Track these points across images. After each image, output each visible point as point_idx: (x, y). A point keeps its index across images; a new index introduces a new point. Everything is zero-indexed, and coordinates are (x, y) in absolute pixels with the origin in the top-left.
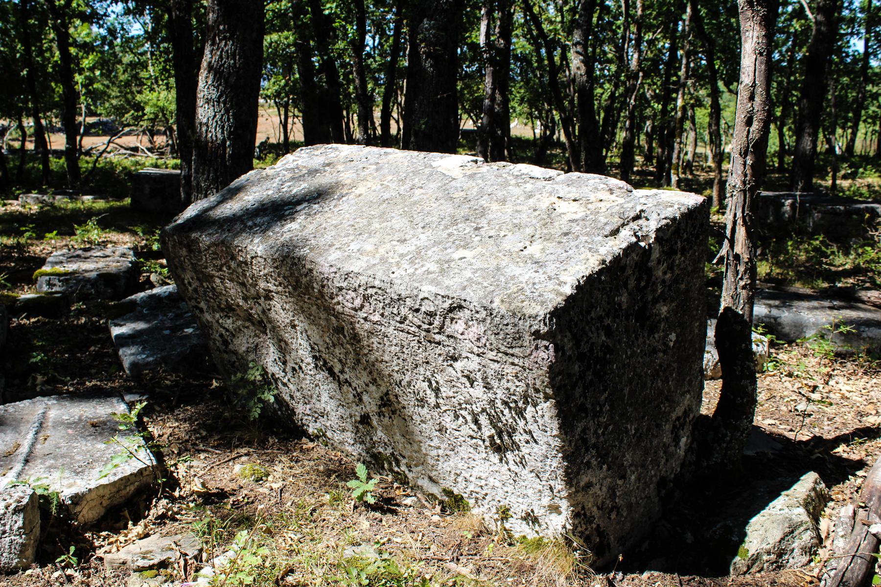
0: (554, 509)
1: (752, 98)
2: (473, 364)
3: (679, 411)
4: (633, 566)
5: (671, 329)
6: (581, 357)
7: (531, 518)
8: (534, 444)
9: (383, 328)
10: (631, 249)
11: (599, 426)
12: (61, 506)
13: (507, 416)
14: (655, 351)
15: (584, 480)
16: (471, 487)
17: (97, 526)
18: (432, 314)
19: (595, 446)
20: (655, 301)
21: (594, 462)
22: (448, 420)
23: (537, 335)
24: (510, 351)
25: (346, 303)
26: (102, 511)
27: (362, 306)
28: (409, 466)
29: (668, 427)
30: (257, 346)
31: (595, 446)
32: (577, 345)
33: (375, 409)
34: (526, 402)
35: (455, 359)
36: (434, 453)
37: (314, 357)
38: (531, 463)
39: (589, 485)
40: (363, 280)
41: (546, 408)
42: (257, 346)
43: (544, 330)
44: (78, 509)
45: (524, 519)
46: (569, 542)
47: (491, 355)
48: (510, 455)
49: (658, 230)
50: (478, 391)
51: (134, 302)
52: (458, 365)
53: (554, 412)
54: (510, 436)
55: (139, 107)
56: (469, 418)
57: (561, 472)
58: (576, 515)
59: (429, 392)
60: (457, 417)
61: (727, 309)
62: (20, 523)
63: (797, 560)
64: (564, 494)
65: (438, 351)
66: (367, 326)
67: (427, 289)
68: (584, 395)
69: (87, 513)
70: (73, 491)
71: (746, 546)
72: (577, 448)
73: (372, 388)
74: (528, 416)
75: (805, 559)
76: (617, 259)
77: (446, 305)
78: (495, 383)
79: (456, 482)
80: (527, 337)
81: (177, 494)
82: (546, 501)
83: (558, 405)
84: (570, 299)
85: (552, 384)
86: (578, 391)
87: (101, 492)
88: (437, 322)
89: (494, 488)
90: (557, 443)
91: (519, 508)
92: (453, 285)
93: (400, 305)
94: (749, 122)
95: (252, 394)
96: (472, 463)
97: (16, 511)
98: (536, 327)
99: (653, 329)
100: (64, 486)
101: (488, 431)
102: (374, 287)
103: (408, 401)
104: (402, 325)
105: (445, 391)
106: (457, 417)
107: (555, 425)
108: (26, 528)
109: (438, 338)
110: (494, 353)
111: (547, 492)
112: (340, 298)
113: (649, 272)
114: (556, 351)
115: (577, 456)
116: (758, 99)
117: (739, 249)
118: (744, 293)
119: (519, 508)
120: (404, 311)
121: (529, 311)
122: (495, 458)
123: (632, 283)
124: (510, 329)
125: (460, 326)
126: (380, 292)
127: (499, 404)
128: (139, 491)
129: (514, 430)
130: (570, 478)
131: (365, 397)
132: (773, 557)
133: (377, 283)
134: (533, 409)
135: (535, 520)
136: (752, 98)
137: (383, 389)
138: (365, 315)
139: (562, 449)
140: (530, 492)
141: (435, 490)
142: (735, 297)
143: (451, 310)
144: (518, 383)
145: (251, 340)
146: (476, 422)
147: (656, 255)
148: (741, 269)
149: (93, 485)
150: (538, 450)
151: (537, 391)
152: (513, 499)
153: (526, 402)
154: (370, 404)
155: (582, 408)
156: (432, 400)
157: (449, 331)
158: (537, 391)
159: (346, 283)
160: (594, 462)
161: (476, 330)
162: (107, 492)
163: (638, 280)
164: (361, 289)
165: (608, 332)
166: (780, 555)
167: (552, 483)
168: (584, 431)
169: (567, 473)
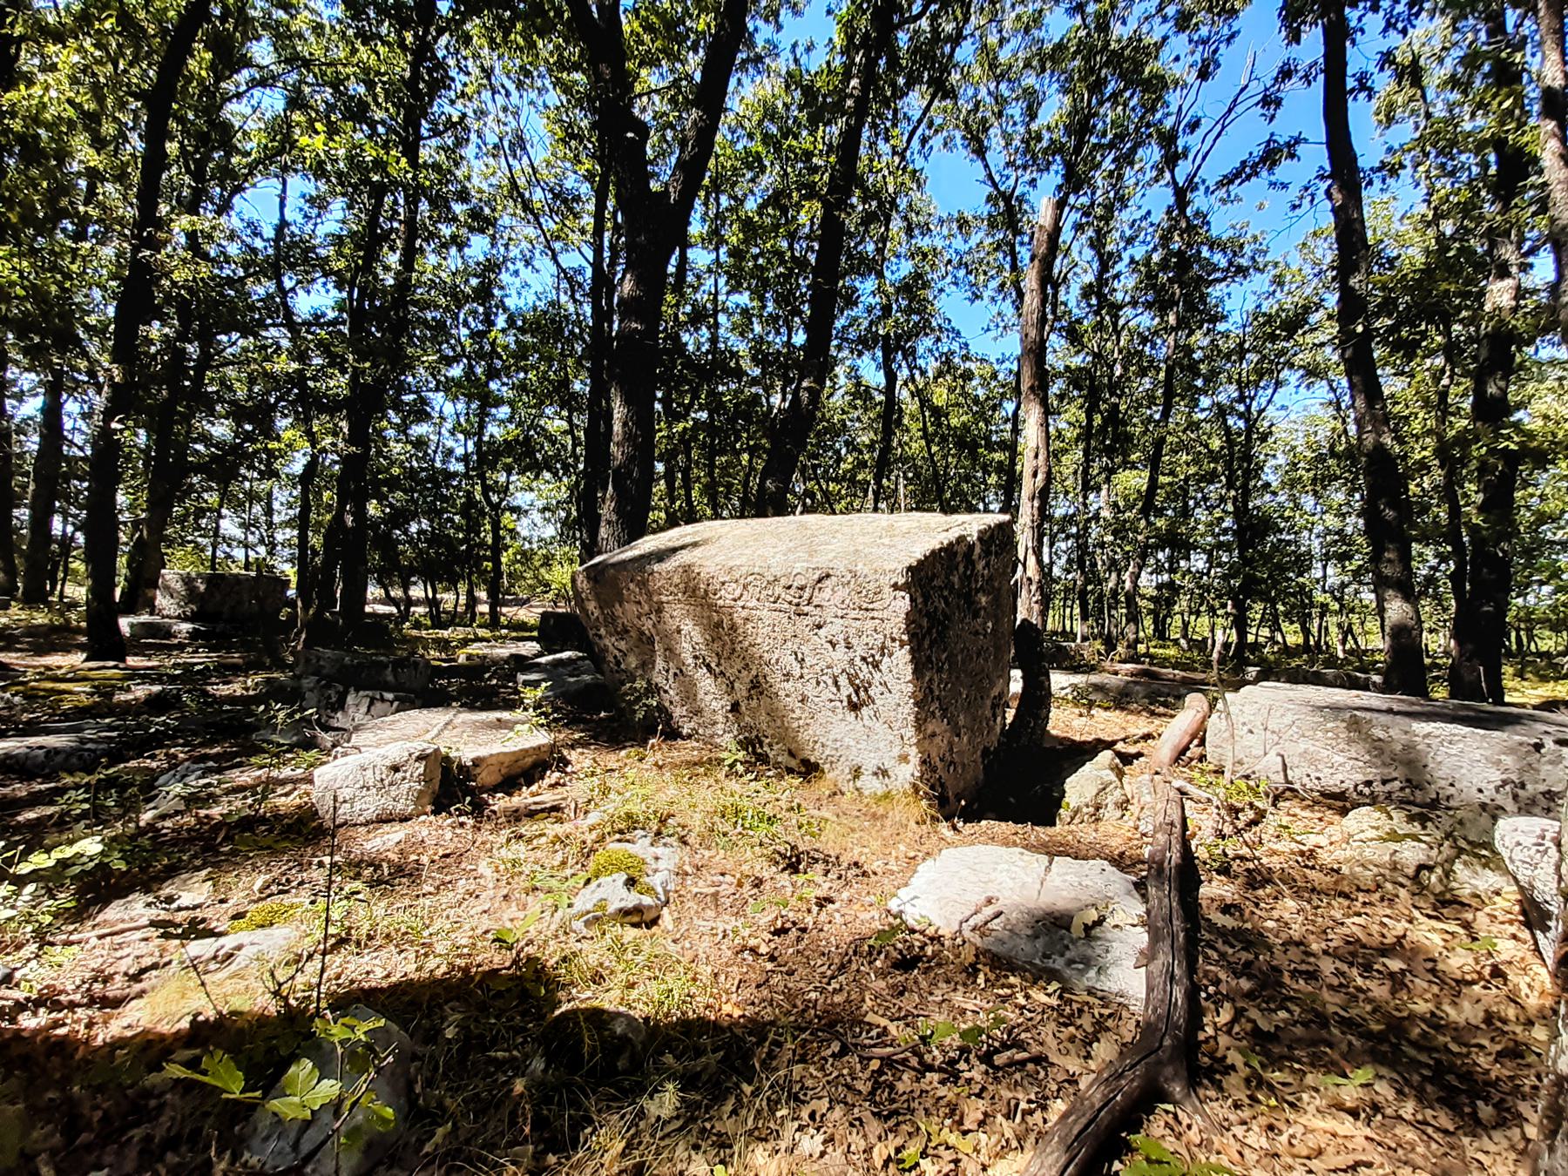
0: (904, 758)
1: (1036, 456)
2: (834, 629)
3: (995, 692)
4: (971, 816)
5: (987, 618)
6: (928, 614)
7: (883, 773)
10: (961, 539)
11: (941, 680)
12: (461, 767)
13: (865, 671)
14: (977, 633)
15: (930, 728)
16: (827, 752)
17: (493, 790)
18: (802, 588)
19: (938, 698)
20: (977, 591)
21: (938, 714)
22: (810, 690)
23: (895, 587)
26: (500, 779)
28: (770, 745)
29: (989, 703)
31: (938, 698)
32: (925, 603)
33: (745, 694)
34: (883, 655)
35: (819, 627)
36: (795, 725)
37: (696, 657)
38: (884, 715)
39: (934, 735)
40: (744, 570)
41: (902, 656)
43: (901, 581)
44: (478, 770)
45: (875, 774)
46: (916, 789)
47: (853, 614)
48: (865, 710)
49: (980, 532)
50: (840, 653)
51: (539, 664)
52: (822, 632)
53: (909, 657)
54: (866, 690)
55: (547, 585)
56: (830, 682)
57: (912, 717)
58: (923, 762)
59: (795, 663)
60: (818, 683)
61: (1024, 621)
62: (421, 770)
63: (1111, 813)
64: (914, 740)
66: (744, 614)
67: (799, 567)
68: (930, 647)
69: (486, 777)
70: (473, 755)
71: (1067, 799)
72: (925, 696)
73: (745, 673)
74: (883, 667)
75: (1119, 813)
76: (951, 544)
77: (816, 577)
78: (854, 641)
79: (813, 750)
80: (887, 590)
81: (569, 769)
82: (896, 751)
83: (912, 651)
84: (919, 562)
85: (907, 631)
86: (926, 643)
87: (501, 758)
88: (806, 595)
89: (848, 747)
90: (911, 688)
91: (869, 766)
92: (823, 561)
94: (1035, 475)
95: (638, 699)
96: (830, 727)
97: (419, 759)
99: (976, 615)
100: (466, 753)
101: (846, 690)
103: (775, 678)
105: (809, 661)
106: (818, 683)
107: (910, 668)
108: (426, 778)
109: (806, 609)
111: (898, 741)
113: (973, 563)
114: (912, 600)
115: (927, 703)
116: (1041, 457)
117: (1029, 574)
118: (1036, 607)
119: (869, 766)
120: (778, 590)
121: (887, 568)
122: (851, 716)
123: (961, 569)
124: (872, 586)
125: (827, 594)
127: (858, 661)
128: (535, 765)
129: (870, 684)
130: (919, 725)
131: (736, 685)
132: (1091, 810)
133: (756, 570)
135: (885, 773)
136: (1036, 456)
137: (754, 673)
139: (913, 695)
140: (881, 745)
141: (793, 763)
142: (1030, 610)
143: (819, 581)
146: (836, 683)
147: (977, 550)
148: (1033, 588)
149: (494, 752)
150: (891, 700)
151: (893, 640)
152: (865, 754)
153: (883, 655)
154: (741, 689)
155: (929, 659)
156: (797, 672)
157: (816, 601)
158: (893, 640)
160: (938, 714)
161: (842, 593)
162: (507, 761)
163: (966, 568)
165: (947, 603)
166: (1098, 809)
168: (931, 680)
169: (917, 719)
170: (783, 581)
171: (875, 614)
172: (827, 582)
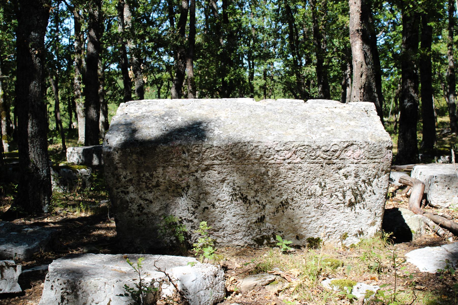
8: (374, 196)
9: (300, 165)
24: (375, 157)
27: (291, 157)
30: (167, 205)
42: (167, 205)
65: (332, 167)
74: (373, 184)
80: (384, 150)
98: (388, 145)
110: (365, 160)
126: (307, 147)
133: (306, 143)
134: (377, 180)
144: (374, 170)
145: (164, 202)
164: (294, 148)
167: (376, 211)
170: (323, 148)
171: (376, 160)
172: (352, 148)
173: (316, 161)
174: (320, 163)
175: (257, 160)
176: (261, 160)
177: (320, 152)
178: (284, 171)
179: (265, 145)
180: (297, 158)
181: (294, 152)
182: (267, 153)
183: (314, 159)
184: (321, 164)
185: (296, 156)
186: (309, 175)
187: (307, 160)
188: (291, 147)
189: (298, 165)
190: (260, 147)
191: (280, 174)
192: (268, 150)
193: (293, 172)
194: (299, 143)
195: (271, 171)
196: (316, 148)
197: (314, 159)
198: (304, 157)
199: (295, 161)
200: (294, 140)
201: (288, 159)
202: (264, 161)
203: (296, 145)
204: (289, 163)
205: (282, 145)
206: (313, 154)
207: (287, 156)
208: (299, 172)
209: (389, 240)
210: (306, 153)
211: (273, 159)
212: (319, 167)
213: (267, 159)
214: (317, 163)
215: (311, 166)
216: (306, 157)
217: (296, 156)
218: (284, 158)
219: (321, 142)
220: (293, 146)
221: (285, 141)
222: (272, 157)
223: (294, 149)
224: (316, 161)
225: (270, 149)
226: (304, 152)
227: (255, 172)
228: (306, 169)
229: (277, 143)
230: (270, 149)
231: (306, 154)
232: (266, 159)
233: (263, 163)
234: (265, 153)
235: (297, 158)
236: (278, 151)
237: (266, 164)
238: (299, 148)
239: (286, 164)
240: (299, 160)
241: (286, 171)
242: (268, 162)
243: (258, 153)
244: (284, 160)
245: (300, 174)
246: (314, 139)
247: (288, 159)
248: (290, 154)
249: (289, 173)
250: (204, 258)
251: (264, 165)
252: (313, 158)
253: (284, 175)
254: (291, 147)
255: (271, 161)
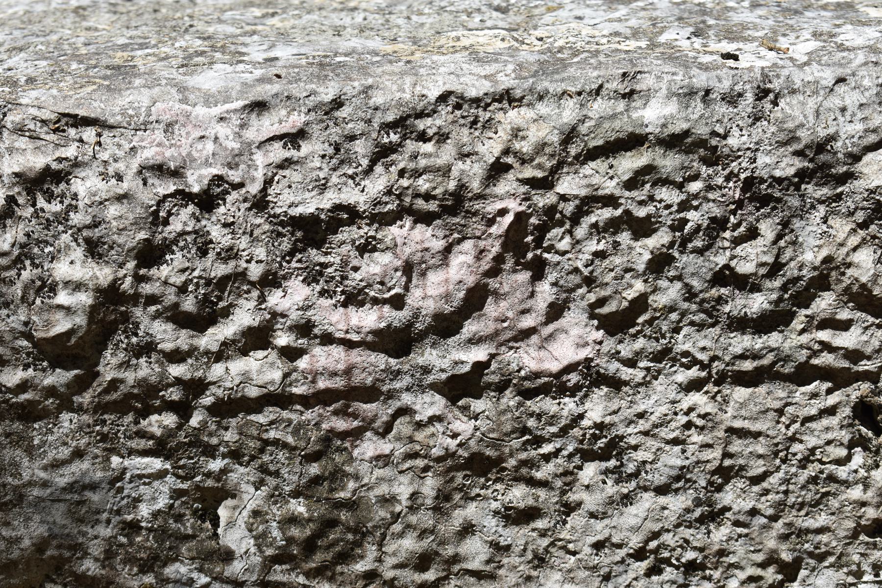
9: (596, 408)
25: (334, 318)
27: (476, 299)
93: (802, 213)
102: (633, 141)
104: (774, 339)
112: (293, 297)
126: (669, 162)
133: (654, 114)
138: (480, 354)
159: (377, 184)
164: (506, 185)
173: (789, 341)
174: (839, 379)
175: (55, 351)
176: (109, 366)
177: (841, 227)
178: (403, 489)
179: (149, 155)
180: (555, 311)
181: (513, 242)
182: (177, 259)
183: (763, 324)
184: (859, 390)
185: (546, 292)
186: (720, 534)
187: (683, 343)
188: (473, 172)
189: (569, 406)
190: (86, 185)
191: (361, 533)
192: (182, 220)
193: (519, 495)
194: (569, 113)
195: (252, 498)
196: (788, 167)
197: (763, 324)
198: (640, 304)
199: (528, 359)
200: (506, 81)
201: (446, 326)
202: (145, 369)
203: (535, 134)
204: (460, 387)
205: (361, 149)
206: (750, 258)
207: (430, 294)
208: (591, 501)
209: (258, 115)
210: (660, 239)
211: (257, 338)
212: (835, 429)
213: (183, 339)
214: (804, 374)
215: (729, 418)
216: (669, 293)
217: (546, 292)
218: (397, 317)
219: (850, 98)
220: (491, 148)
221: (393, 92)
222: (244, 316)
223: (508, 198)
224: (789, 341)
225: (207, 201)
226: (642, 228)
227: (58, 513)
228: (673, 459)
229: (297, 120)
230: (207, 201)
231: (659, 263)
232: (167, 336)
233: (146, 399)
234: (150, 255)
235: (555, 311)
236: (313, 231)
237: (183, 410)
238: (570, 185)
239: (429, 405)
240: (572, 342)
241: (430, 486)
242: (196, 387)
243: (62, 270)
244: (396, 341)
245: (600, 529)
246: (754, 59)
247: (446, 326)
248: (462, 268)
249: (471, 511)
250: (714, 134)
251: (159, 423)
252: (757, 303)
253: (409, 544)
254: (473, 172)
255: (238, 366)
